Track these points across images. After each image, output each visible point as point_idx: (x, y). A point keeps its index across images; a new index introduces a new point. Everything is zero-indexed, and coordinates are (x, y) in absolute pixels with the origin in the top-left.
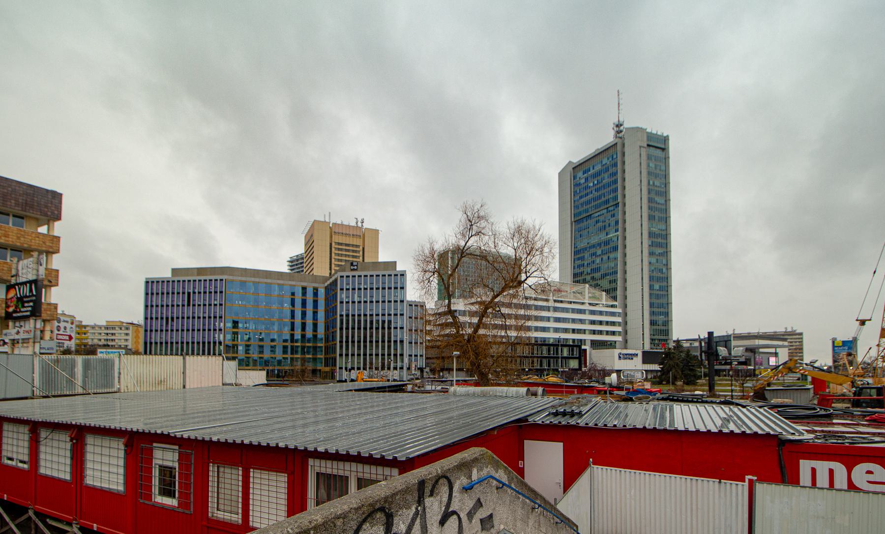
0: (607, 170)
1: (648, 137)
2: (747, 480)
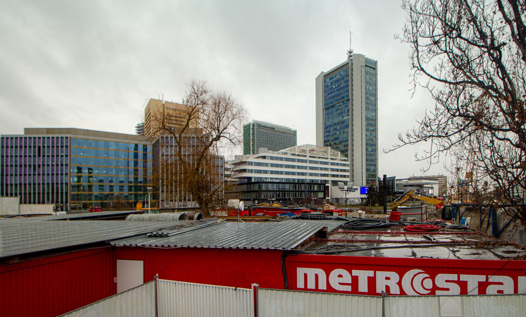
0: (343, 78)
1: (366, 60)
2: (252, 288)
